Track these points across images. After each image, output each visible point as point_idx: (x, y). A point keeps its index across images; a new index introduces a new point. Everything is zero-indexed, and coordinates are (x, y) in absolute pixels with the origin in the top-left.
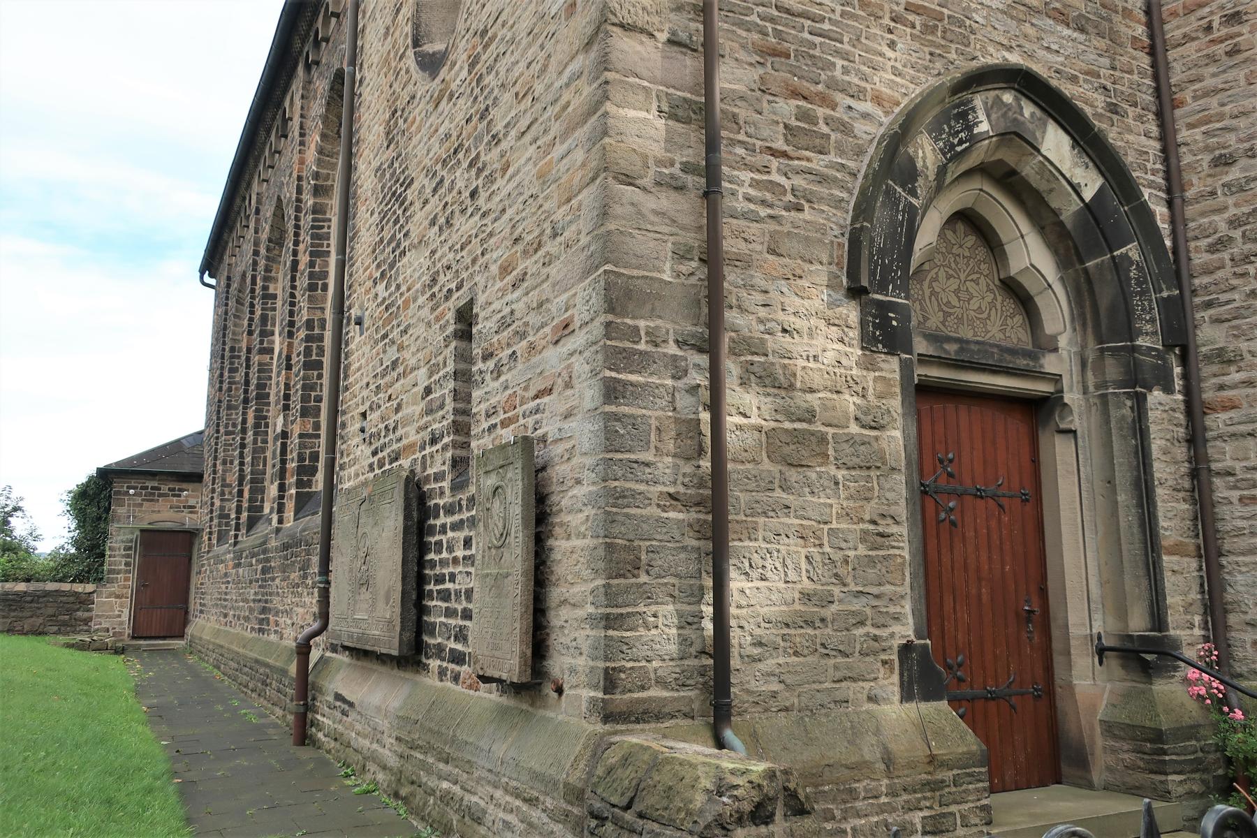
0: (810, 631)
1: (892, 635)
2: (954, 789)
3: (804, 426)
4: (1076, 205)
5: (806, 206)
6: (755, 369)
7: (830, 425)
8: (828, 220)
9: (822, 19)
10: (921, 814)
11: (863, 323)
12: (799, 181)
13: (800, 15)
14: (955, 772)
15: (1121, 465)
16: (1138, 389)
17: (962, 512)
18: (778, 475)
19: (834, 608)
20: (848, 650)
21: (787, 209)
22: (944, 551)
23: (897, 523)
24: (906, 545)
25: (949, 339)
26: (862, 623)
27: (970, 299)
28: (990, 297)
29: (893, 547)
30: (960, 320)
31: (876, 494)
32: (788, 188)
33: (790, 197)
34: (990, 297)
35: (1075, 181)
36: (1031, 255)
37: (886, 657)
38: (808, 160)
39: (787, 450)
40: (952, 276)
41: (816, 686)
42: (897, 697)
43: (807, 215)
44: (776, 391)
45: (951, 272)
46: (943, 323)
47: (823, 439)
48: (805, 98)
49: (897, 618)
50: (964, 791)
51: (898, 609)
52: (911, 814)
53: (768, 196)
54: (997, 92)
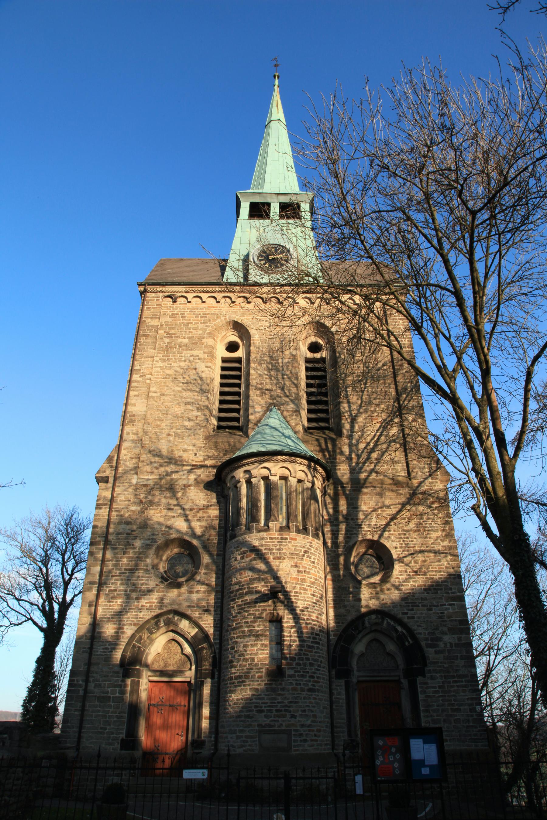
47: (110, 697)
49: (121, 733)
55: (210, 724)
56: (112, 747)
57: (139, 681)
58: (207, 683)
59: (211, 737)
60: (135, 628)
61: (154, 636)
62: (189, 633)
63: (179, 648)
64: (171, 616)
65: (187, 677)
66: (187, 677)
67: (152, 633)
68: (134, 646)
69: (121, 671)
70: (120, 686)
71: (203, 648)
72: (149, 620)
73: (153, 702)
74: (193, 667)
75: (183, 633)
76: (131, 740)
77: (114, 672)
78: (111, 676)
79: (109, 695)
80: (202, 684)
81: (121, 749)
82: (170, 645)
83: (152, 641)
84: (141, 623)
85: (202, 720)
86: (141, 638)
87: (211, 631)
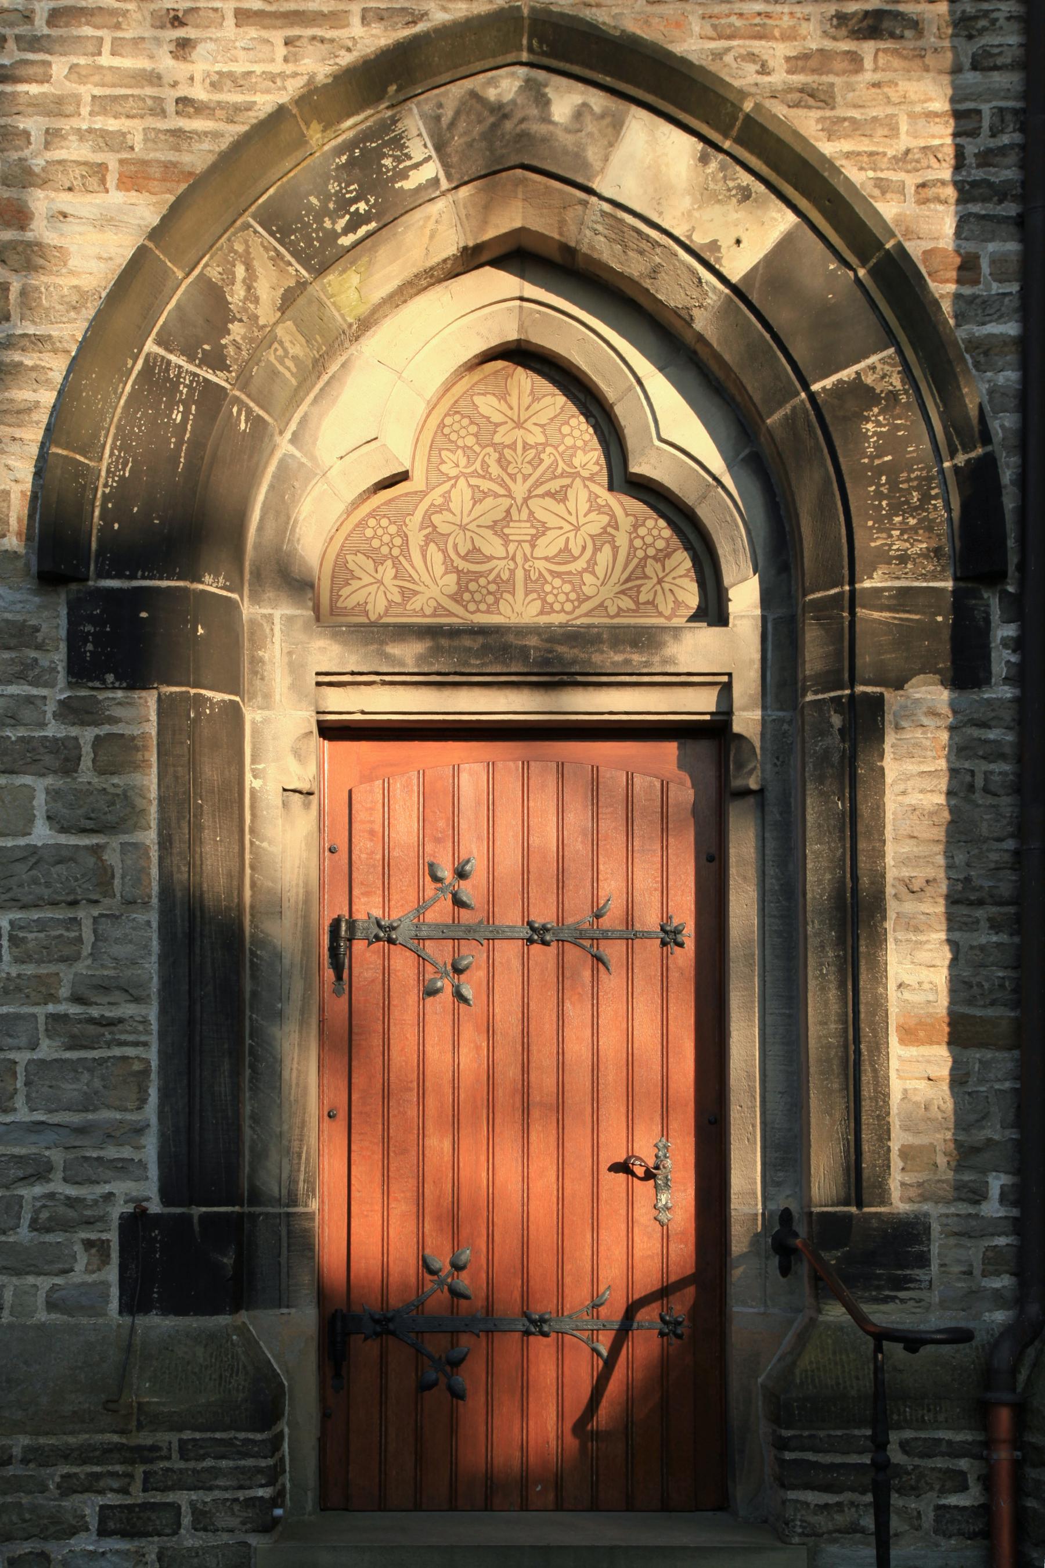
1: (109, 1197)
2: (182, 1465)
10: (101, 1500)
11: (74, 640)
15: (818, 854)
23: (137, 1000)
24: (154, 1040)
29: (125, 1044)
30: (504, 586)
31: (86, 949)
35: (699, 239)
37: (93, 1236)
42: (114, 1305)
49: (122, 1168)
51: (126, 1152)
52: (77, 1498)
55: (958, 1080)
56: (44, 1283)
57: (234, 715)
58: (907, 713)
59: (976, 1195)
60: (145, 210)
61: (347, 291)
63: (579, 431)
64: (506, 86)
65: (685, 681)
66: (685, 681)
67: (322, 258)
68: (157, 381)
69: (53, 620)
70: (64, 758)
71: (860, 394)
72: (280, 113)
73: (368, 907)
74: (745, 596)
75: (632, 266)
76: (212, 1234)
80: (864, 725)
82: (487, 405)
83: (330, 345)
84: (198, 158)
85: (880, 1047)
86: (215, 307)
87: (926, 222)
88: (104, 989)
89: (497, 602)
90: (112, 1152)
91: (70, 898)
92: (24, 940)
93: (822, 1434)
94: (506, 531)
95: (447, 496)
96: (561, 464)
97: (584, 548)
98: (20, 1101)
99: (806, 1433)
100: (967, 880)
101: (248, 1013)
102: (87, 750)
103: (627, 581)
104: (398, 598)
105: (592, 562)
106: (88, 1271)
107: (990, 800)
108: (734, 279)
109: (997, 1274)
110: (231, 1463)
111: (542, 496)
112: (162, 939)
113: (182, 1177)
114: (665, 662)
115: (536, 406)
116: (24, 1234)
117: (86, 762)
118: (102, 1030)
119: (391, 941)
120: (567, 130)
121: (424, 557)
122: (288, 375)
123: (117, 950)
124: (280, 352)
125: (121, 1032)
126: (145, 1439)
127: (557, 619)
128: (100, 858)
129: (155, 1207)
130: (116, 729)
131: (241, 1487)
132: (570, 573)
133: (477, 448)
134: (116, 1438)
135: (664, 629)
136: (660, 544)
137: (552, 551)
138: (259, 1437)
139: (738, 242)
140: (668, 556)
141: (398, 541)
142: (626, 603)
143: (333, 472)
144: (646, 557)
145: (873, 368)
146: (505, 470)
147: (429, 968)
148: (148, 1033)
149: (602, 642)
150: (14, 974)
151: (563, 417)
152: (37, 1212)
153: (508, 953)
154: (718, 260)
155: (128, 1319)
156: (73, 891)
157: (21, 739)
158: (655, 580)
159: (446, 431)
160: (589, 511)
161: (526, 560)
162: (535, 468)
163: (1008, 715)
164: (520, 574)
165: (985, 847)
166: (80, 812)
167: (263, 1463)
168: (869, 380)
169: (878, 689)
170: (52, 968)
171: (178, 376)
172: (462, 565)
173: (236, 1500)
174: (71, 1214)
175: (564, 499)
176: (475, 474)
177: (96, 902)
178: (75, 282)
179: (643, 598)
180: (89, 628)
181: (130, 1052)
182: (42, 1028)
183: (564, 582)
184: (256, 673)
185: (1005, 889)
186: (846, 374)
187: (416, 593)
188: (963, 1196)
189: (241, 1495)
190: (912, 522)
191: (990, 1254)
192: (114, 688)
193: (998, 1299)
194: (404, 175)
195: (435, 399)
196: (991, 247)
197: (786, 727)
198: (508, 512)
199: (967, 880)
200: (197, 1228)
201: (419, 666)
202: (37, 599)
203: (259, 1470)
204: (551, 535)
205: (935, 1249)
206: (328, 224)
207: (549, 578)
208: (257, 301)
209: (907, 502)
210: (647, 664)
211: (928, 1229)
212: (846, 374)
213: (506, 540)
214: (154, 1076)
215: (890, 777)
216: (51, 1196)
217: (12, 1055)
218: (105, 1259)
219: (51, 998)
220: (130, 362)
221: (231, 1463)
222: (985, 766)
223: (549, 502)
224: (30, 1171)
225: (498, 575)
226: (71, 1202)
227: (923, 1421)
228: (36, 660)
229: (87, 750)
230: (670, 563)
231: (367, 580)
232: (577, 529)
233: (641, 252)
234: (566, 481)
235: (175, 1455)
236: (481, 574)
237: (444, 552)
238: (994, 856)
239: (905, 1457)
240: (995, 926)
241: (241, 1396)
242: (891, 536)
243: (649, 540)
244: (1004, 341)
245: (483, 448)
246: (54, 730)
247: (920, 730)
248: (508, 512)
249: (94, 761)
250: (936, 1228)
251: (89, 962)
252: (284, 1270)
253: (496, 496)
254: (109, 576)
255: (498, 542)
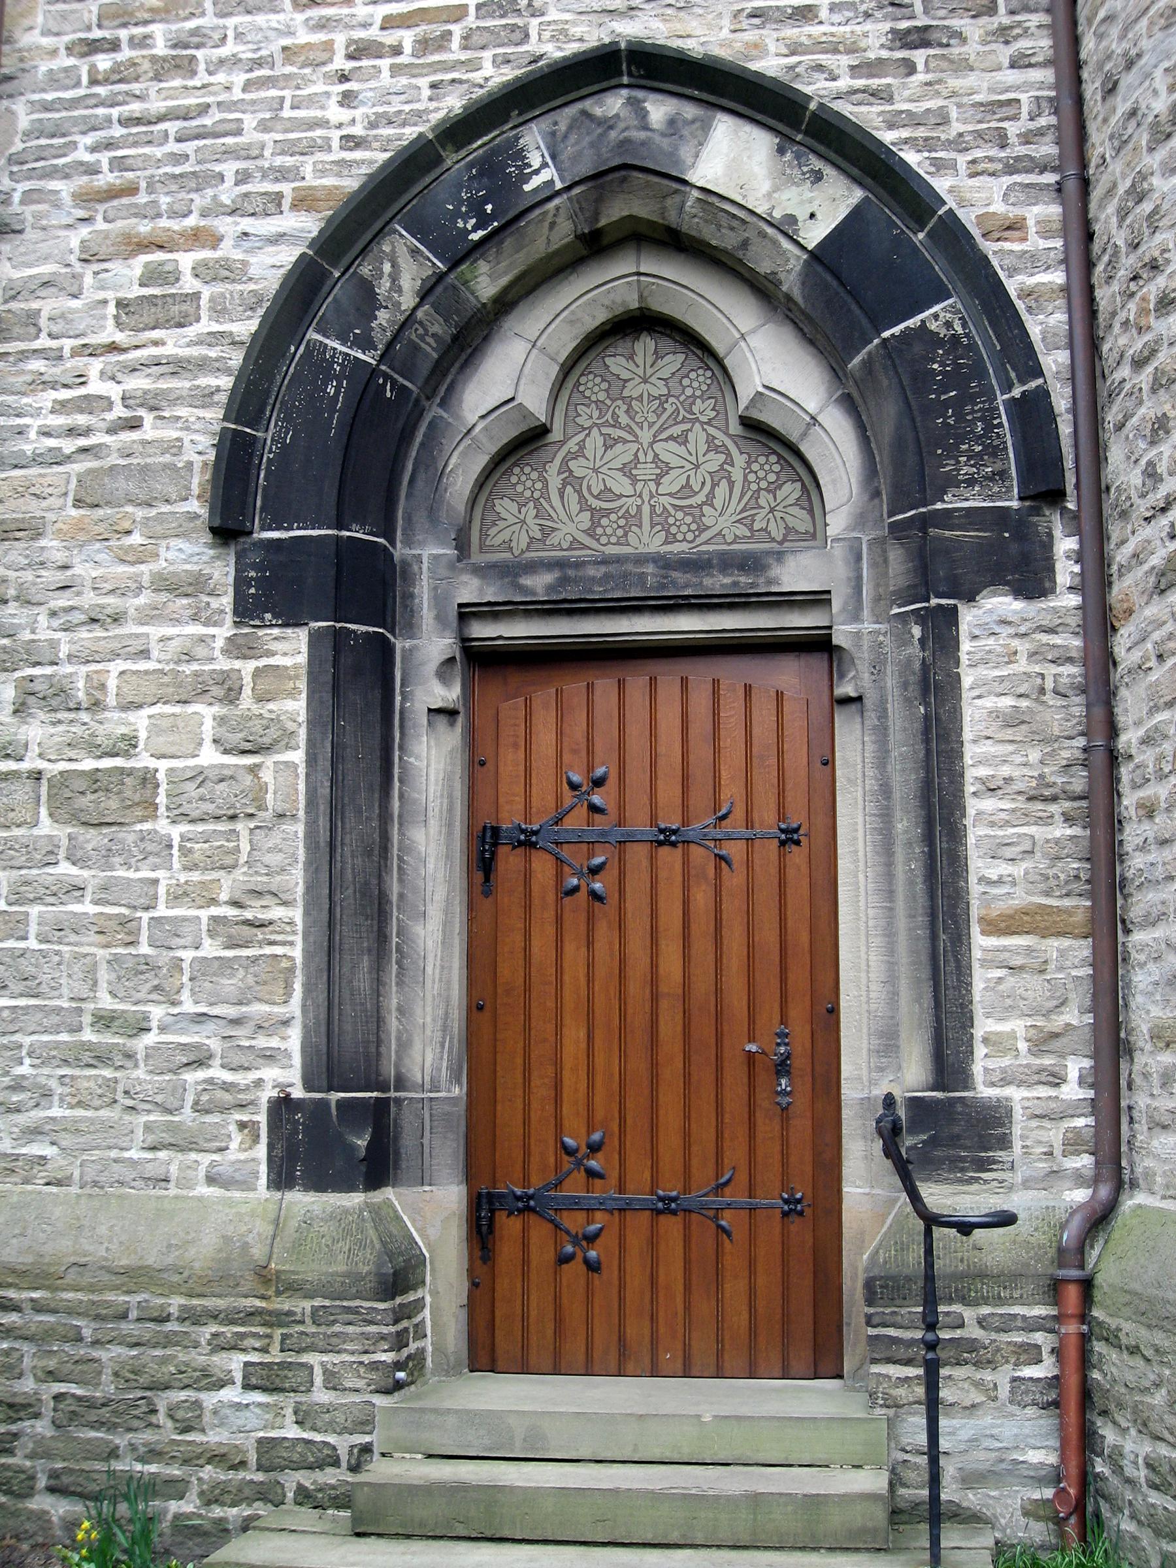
0: (107, 1073)
1: (259, 1083)
2: (313, 1329)
3: (118, 762)
4: (795, 260)
5: (148, 418)
6: (38, 686)
7: (164, 756)
8: (188, 429)
9: (204, 109)
11: (240, 583)
12: (138, 383)
13: (161, 119)
14: (318, 1302)
16: (934, 601)
17: (622, 874)
18: (65, 842)
19: (150, 1039)
20: (173, 1103)
21: (111, 431)
22: (570, 948)
23: (285, 903)
24: (298, 939)
25: (532, 567)
26: (200, 1063)
27: (660, 476)
28: (715, 461)
30: (632, 519)
31: (243, 858)
32: (116, 397)
33: (119, 411)
34: (715, 461)
36: (774, 366)
38: (156, 343)
39: (84, 801)
40: (618, 440)
41: (114, 1154)
42: (263, 1180)
43: (150, 430)
44: (72, 715)
45: (616, 433)
46: (590, 532)
47: (147, 779)
48: (161, 247)
49: (269, 1057)
50: (336, 1335)
51: (274, 1042)
53: (81, 420)
54: (579, 106)
56: (206, 1159)
59: (1056, 1079)
62: (787, 227)
69: (222, 571)
77: (168, 585)
78: (150, 616)
79: (143, 761)
81: (281, 1179)
88: (258, 894)
89: (626, 534)
90: (262, 1042)
91: (231, 812)
92: (190, 851)
93: (903, 1311)
94: (634, 472)
95: (582, 445)
96: (682, 412)
97: (703, 483)
98: (185, 996)
99: (888, 1311)
100: (1042, 776)
101: (395, 913)
102: (247, 680)
103: (742, 511)
104: (538, 535)
105: (711, 495)
106: (240, 1150)
107: (1061, 702)
108: (810, 247)
109: (1078, 1153)
110: (358, 1330)
111: (666, 440)
112: (308, 848)
113: (326, 1065)
114: (769, 582)
115: (660, 363)
116: (187, 1115)
117: (247, 691)
118: (255, 930)
119: (533, 845)
120: (663, 135)
121: (562, 498)
122: (429, 349)
123: (269, 859)
124: (421, 331)
125: (272, 933)
126: (284, 1304)
127: (676, 548)
128: (256, 776)
129: (298, 1093)
130: (272, 661)
131: (366, 1352)
132: (691, 506)
133: (608, 402)
134: (258, 1303)
135: (768, 553)
136: (772, 477)
137: (675, 488)
138: (381, 1306)
139: (812, 216)
140: (780, 487)
141: (539, 485)
142: (743, 531)
143: (477, 429)
144: (760, 489)
145: (936, 316)
146: (633, 419)
147: (566, 869)
148: (294, 933)
149: (711, 567)
150: (182, 881)
151: (684, 371)
152: (198, 1094)
153: (638, 854)
154: (796, 231)
155: (279, 1195)
156: (233, 806)
157: (196, 674)
158: (767, 509)
159: (582, 388)
160: (708, 451)
161: (652, 496)
162: (659, 417)
163: (1074, 621)
164: (646, 509)
165: (1056, 745)
166: (241, 735)
167: (385, 1330)
168: (933, 326)
169: (951, 602)
170: (215, 875)
171: (333, 357)
172: (595, 503)
173: (361, 1363)
174: (227, 1097)
175: (685, 442)
176: (607, 424)
177: (252, 815)
178: (252, 286)
179: (756, 526)
180: (252, 574)
181: (278, 950)
182: (204, 927)
183: (686, 514)
184: (406, 606)
185: (1079, 783)
186: (913, 322)
187: (554, 530)
188: (1043, 1079)
189: (366, 1359)
190: (979, 448)
191: (1070, 1135)
192: (272, 626)
193: (1079, 1179)
194: (527, 179)
195: (570, 363)
196: (1036, 209)
197: (881, 638)
198: (636, 455)
199: (1042, 776)
200: (334, 1112)
201: (548, 594)
202: (212, 552)
203: (383, 1337)
204: (673, 473)
205: (1017, 1131)
206: (460, 224)
207: (673, 512)
208: (400, 290)
209: (972, 432)
210: (752, 585)
211: (1009, 1112)
212: (913, 322)
213: (634, 480)
214: (298, 972)
215: (967, 681)
216: (210, 1081)
217: (180, 953)
218: (256, 1139)
219: (213, 902)
220: (293, 348)
221: (358, 1330)
222: (1055, 669)
223: (672, 446)
224: (192, 1058)
225: (627, 511)
226: (227, 1087)
227: (1000, 1297)
228: (208, 604)
229: (247, 680)
230: (780, 494)
231: (513, 520)
232: (697, 467)
233: (732, 229)
234: (688, 426)
235: (308, 1320)
236: (612, 511)
237: (579, 492)
238: (1066, 754)
239: (982, 1332)
240: (1068, 819)
241: (366, 1269)
242: (958, 462)
243: (761, 474)
244: (1051, 289)
245: (613, 401)
246: (224, 664)
247: (993, 638)
248: (636, 455)
249: (253, 689)
250: (1018, 1114)
251: (245, 869)
252: (427, 1150)
253: (625, 441)
254: (271, 529)
255: (626, 481)
